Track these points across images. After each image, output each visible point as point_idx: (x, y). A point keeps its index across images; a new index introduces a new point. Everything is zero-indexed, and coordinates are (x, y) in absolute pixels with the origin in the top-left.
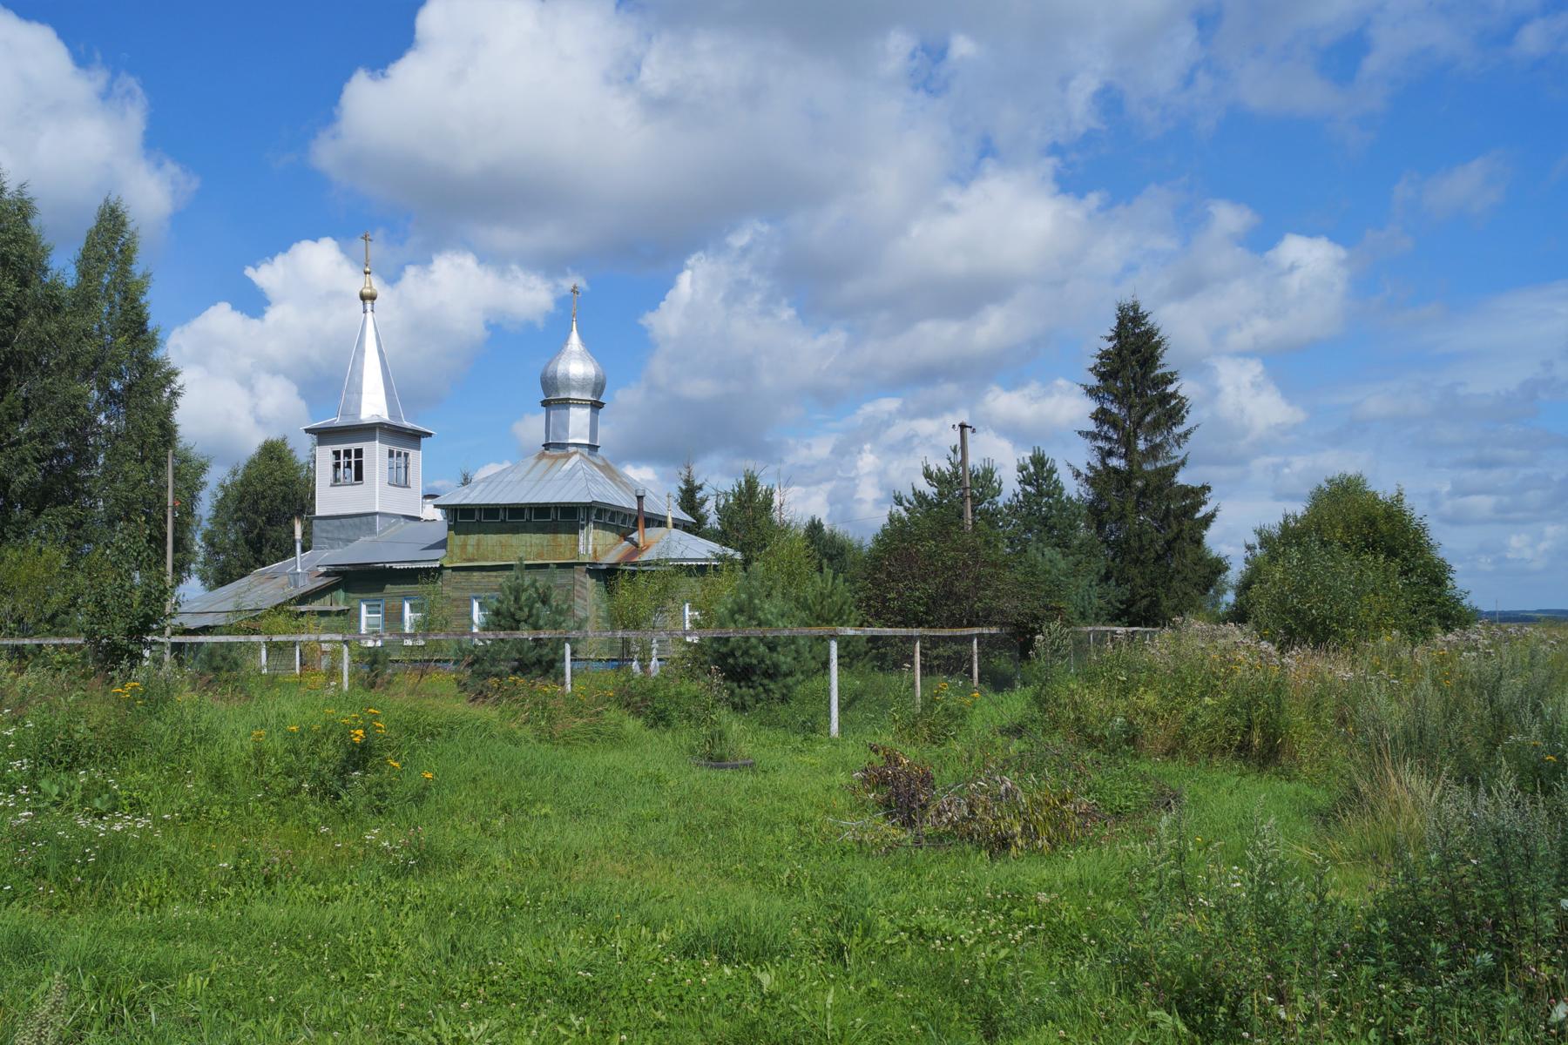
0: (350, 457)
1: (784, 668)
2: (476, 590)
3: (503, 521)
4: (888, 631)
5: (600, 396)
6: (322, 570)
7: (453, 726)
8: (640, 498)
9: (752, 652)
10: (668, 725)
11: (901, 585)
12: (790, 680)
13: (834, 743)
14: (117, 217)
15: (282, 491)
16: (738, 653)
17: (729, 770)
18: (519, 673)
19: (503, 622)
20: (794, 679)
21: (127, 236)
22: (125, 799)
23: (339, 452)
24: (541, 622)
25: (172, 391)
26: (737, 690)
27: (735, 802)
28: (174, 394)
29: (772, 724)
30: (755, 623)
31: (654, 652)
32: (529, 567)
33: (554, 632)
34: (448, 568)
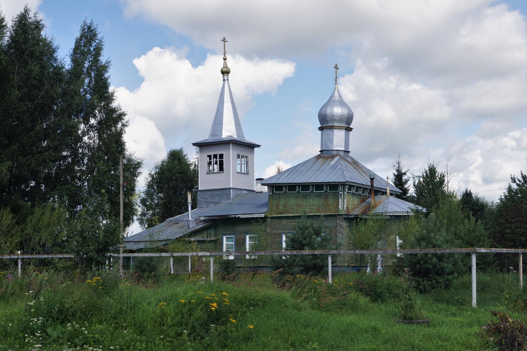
0: (216, 158)
1: (447, 270)
2: (284, 229)
3: (298, 192)
4: (505, 250)
5: (350, 124)
6: (202, 218)
7: (266, 301)
8: (372, 180)
9: (429, 261)
10: (383, 301)
11: (513, 225)
12: (450, 277)
13: (473, 310)
14: (91, 31)
15: (181, 177)
16: (422, 262)
17: (415, 325)
18: (304, 273)
19: (295, 246)
20: (452, 276)
21: (97, 41)
22: (91, 338)
23: (211, 155)
24: (316, 246)
25: (122, 124)
26: (422, 282)
27: (417, 342)
28: (124, 125)
29: (437, 300)
30: (430, 246)
31: (379, 262)
32: (309, 217)
33: (322, 251)
34: (269, 217)
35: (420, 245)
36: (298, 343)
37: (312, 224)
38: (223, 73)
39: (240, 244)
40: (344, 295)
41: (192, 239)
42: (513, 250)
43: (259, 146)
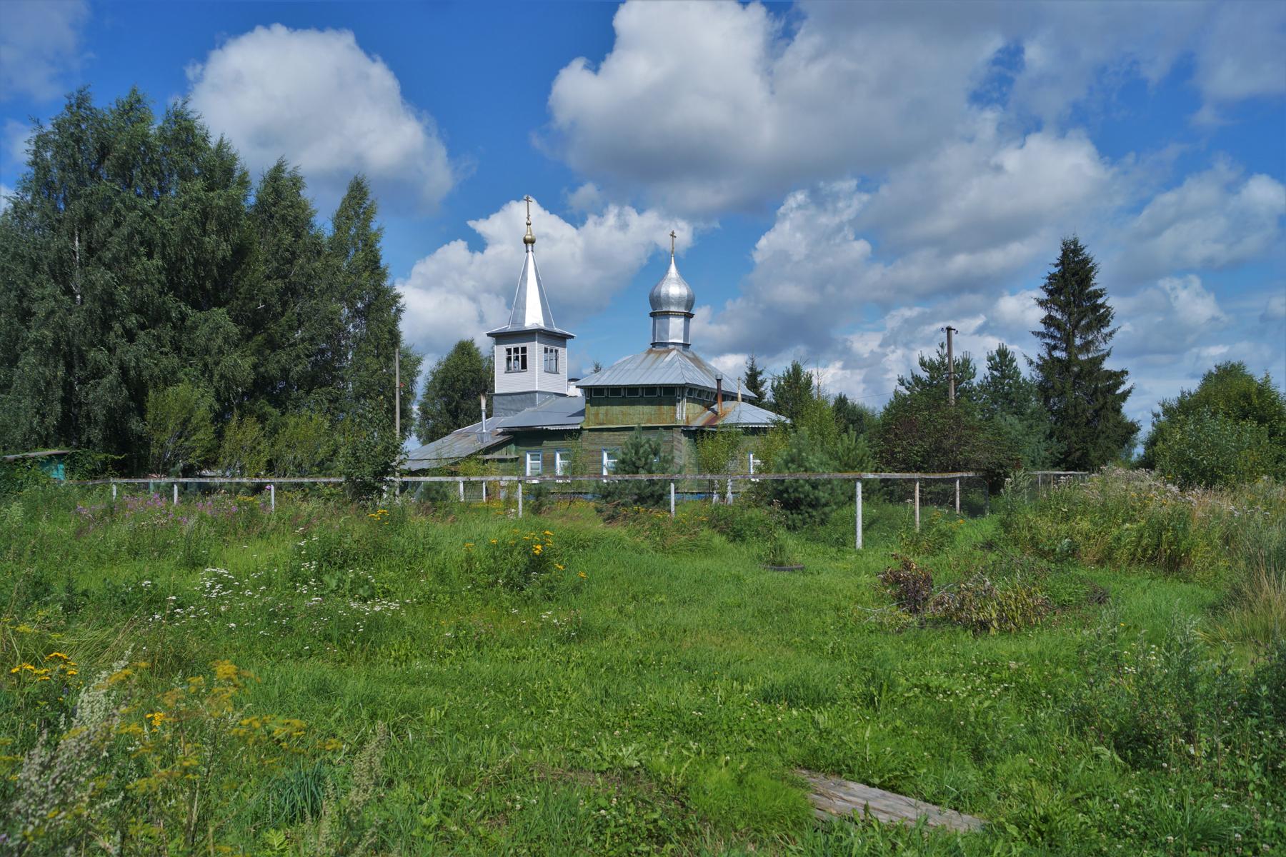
6: (500, 431)
8: (719, 381)
10: (743, 540)
13: (860, 554)
16: (791, 490)
24: (654, 468)
26: (790, 516)
29: (815, 540)
32: (644, 428)
35: (789, 469)
36: (641, 596)
37: (649, 440)
38: (526, 242)
39: (549, 464)
40: (695, 533)
41: (488, 457)
42: (907, 475)
43: (572, 337)
